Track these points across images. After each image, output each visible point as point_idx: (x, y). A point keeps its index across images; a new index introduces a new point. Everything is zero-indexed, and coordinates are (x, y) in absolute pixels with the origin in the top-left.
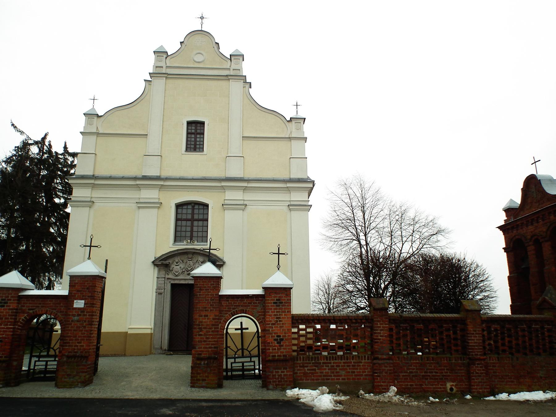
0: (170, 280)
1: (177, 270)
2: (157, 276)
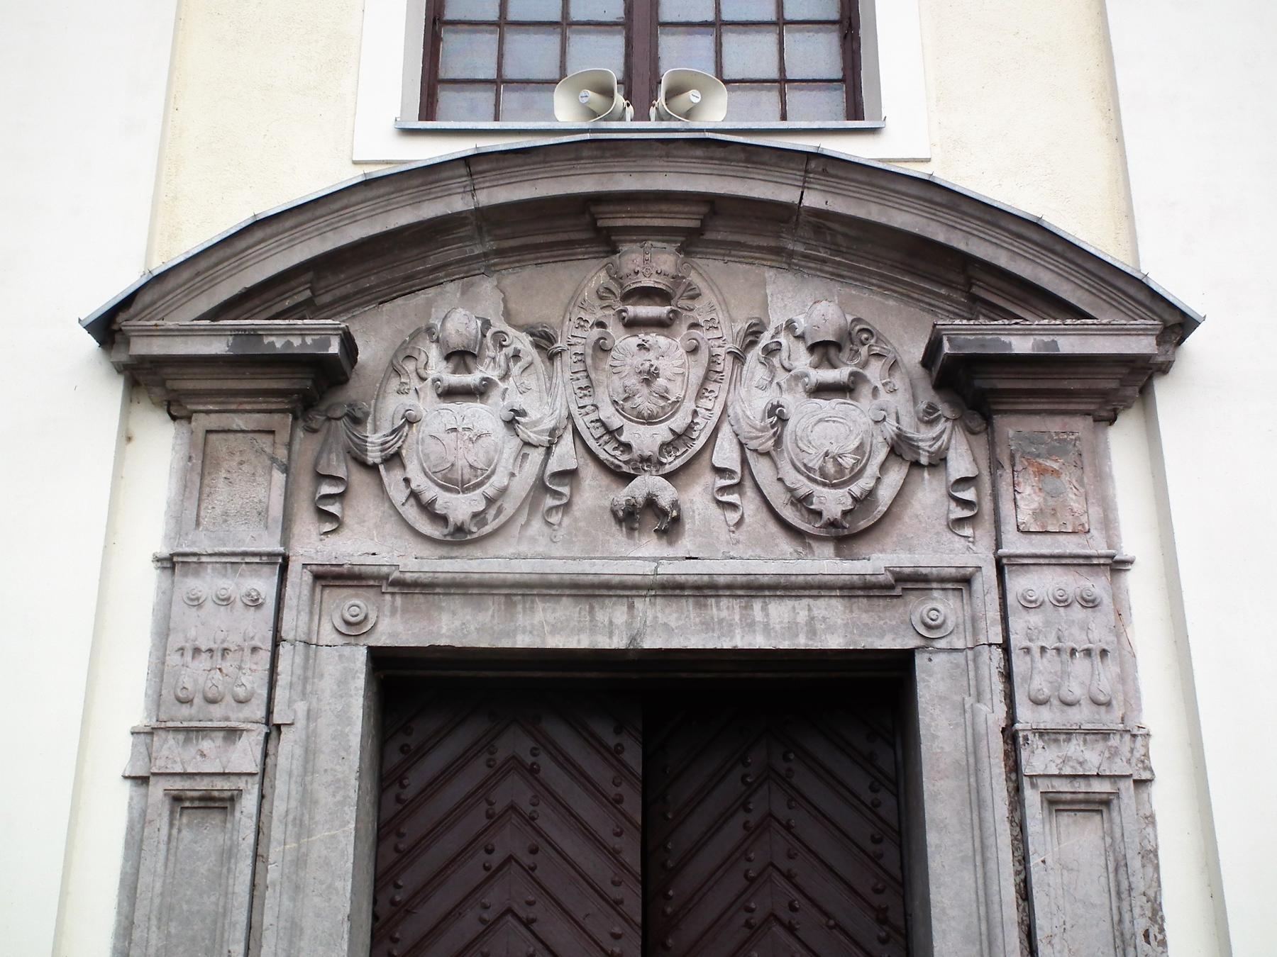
0: (351, 603)
2: (178, 526)
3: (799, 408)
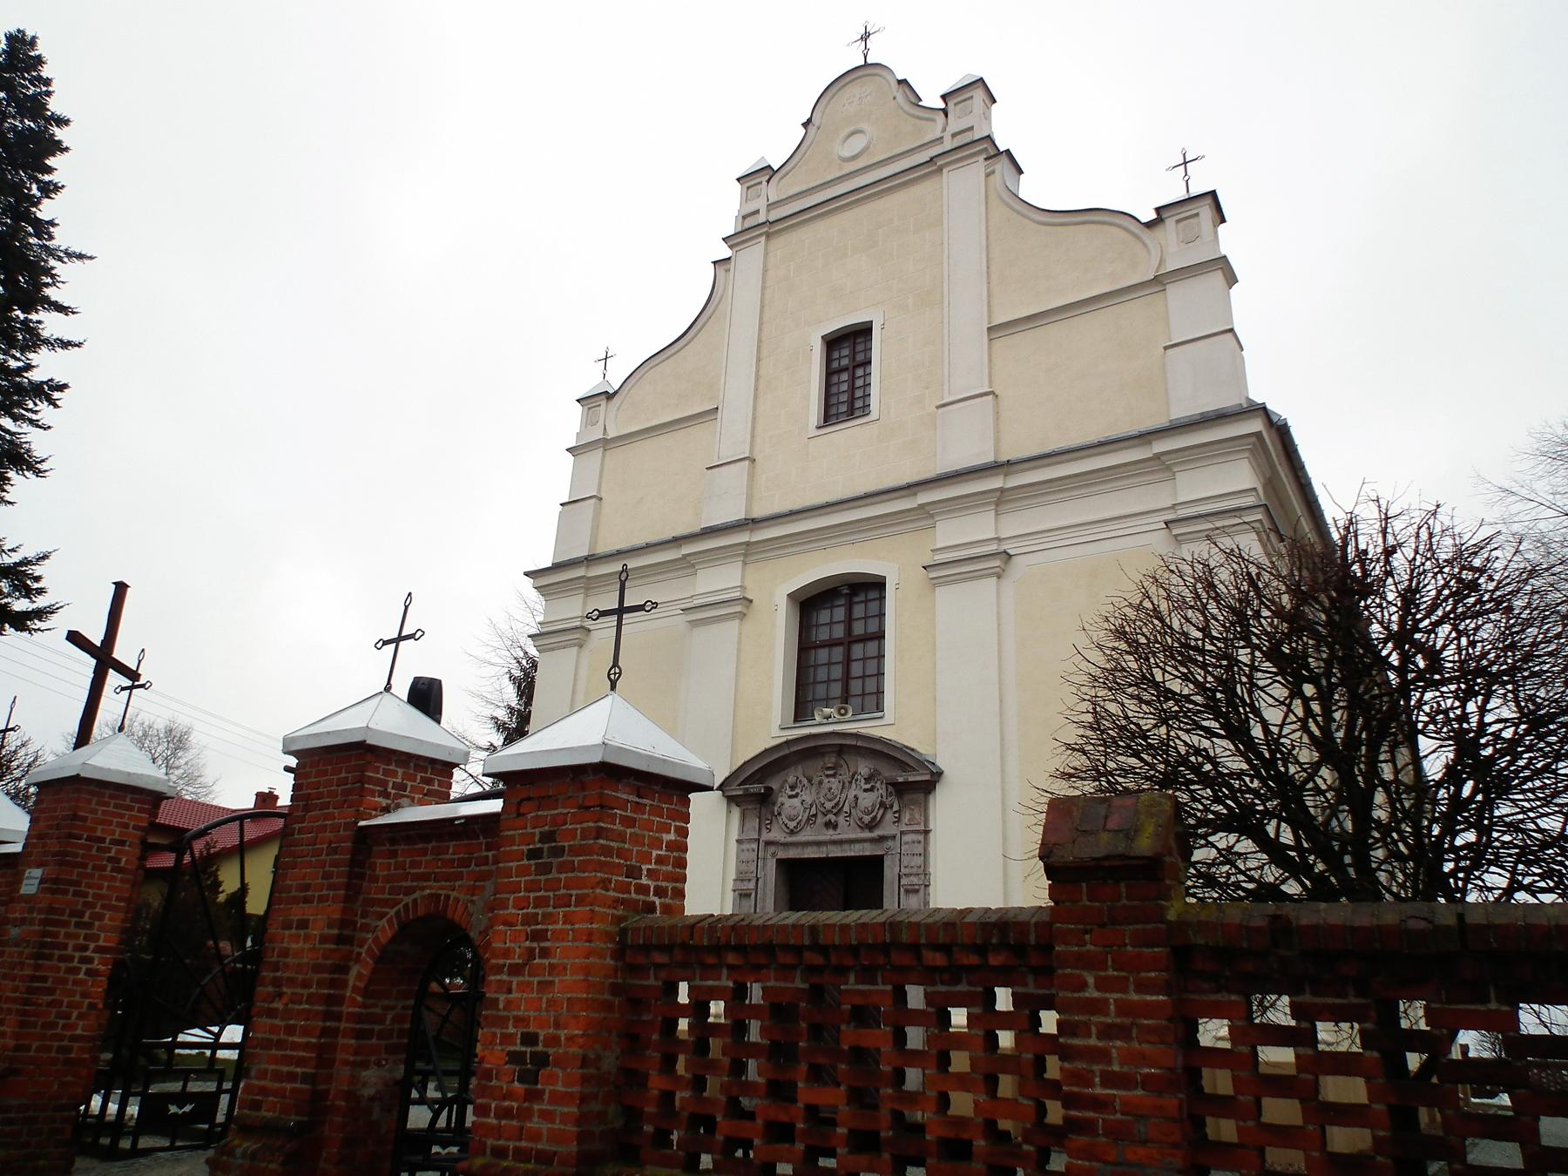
0: (772, 849)
1: (794, 813)
2: (739, 835)
3: (862, 795)
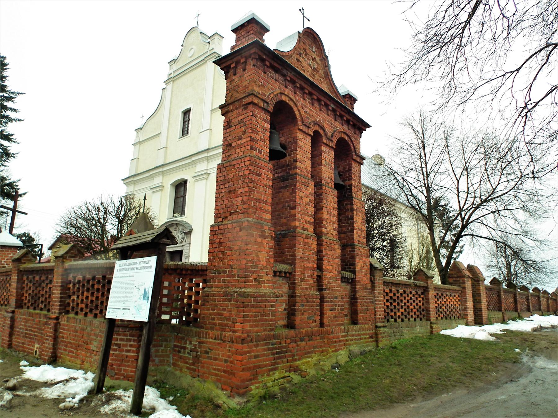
3: (180, 235)
